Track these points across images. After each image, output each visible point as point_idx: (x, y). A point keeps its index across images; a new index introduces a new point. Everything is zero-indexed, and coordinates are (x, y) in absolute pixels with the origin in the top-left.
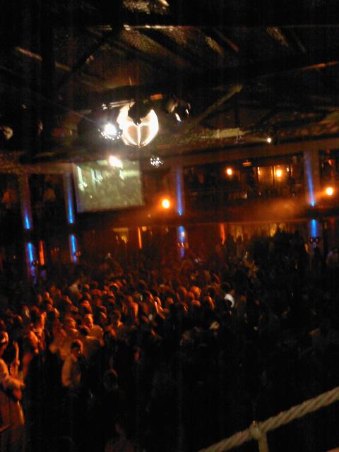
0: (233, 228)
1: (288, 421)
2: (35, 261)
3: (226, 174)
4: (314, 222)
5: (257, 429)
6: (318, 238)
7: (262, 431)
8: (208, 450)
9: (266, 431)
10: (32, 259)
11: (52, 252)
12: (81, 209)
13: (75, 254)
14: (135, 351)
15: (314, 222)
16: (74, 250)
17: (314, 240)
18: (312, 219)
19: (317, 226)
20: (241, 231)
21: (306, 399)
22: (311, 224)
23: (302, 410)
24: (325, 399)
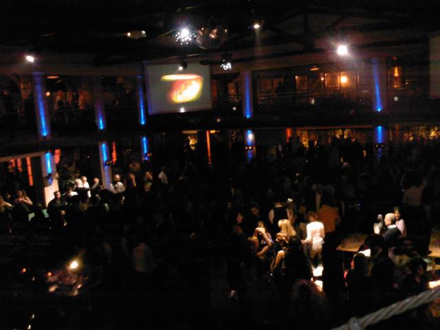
0: (299, 133)
1: (388, 317)
2: (108, 161)
3: (30, 53)
4: (380, 128)
5: (356, 325)
6: (383, 144)
7: (361, 325)
8: (339, 329)
9: (365, 325)
10: (105, 159)
11: (124, 152)
12: (152, 111)
13: (146, 155)
14: (393, 212)
15: (380, 128)
16: (146, 151)
17: (380, 145)
18: (378, 126)
19: (383, 131)
20: (307, 136)
21: (394, 303)
22: (377, 130)
23: (404, 306)
24: (385, 313)
